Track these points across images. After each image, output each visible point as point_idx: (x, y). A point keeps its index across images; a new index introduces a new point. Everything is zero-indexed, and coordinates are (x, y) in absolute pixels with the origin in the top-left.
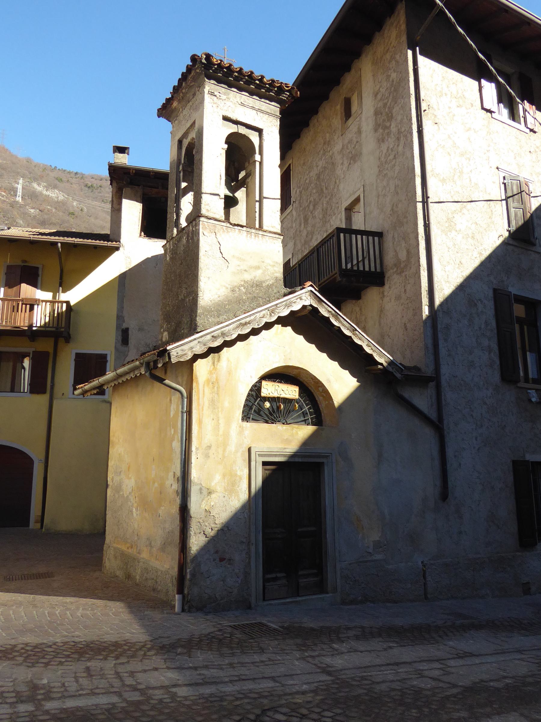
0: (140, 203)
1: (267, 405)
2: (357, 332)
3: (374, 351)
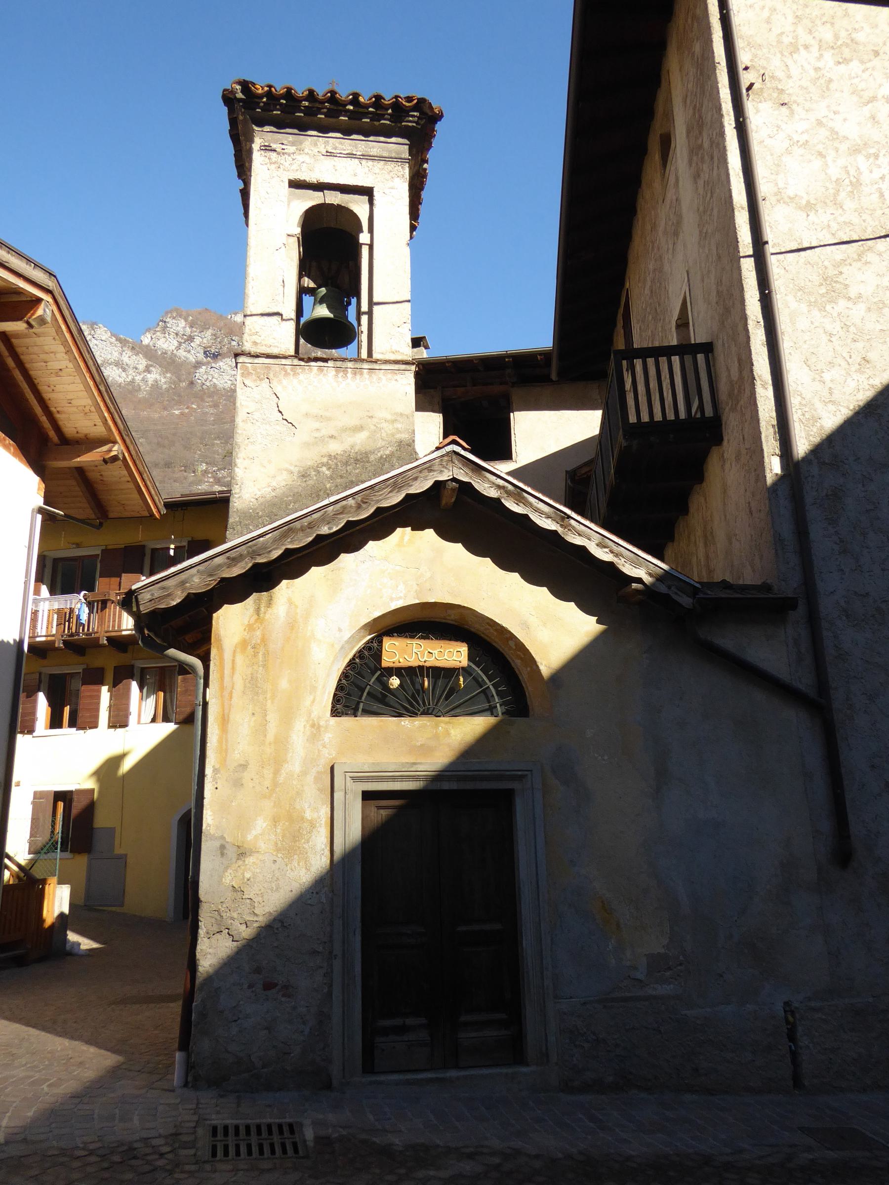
0: (439, 413)
1: (395, 682)
2: (572, 522)
3: (617, 555)
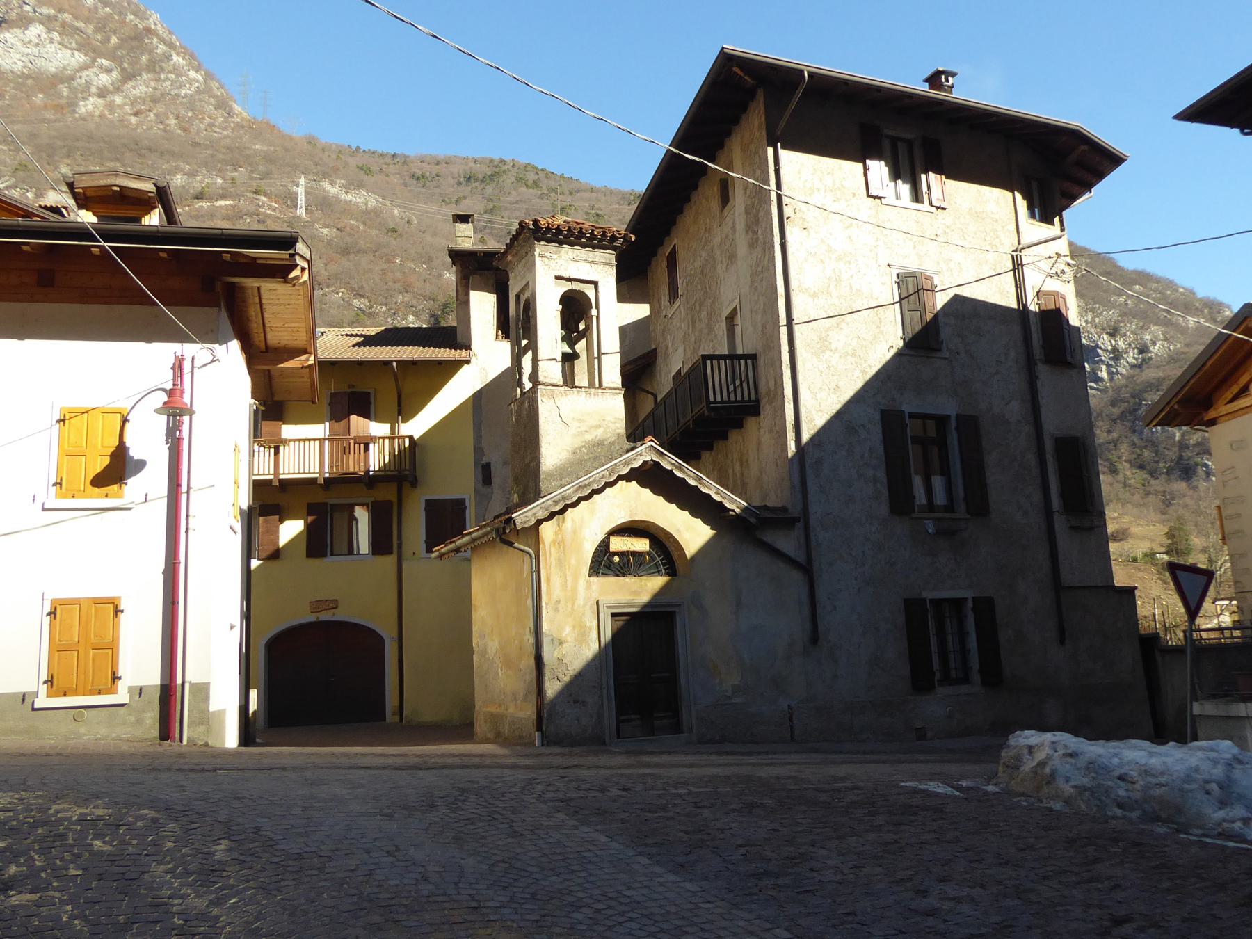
1: (617, 559)
